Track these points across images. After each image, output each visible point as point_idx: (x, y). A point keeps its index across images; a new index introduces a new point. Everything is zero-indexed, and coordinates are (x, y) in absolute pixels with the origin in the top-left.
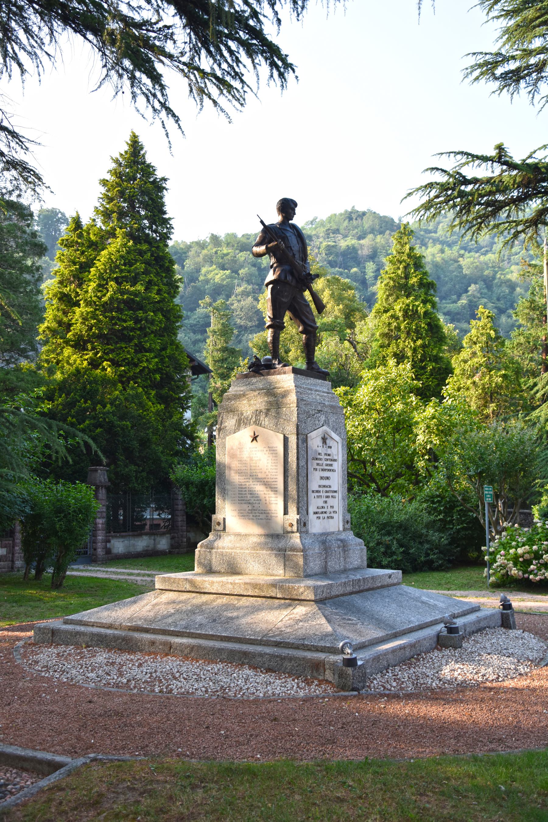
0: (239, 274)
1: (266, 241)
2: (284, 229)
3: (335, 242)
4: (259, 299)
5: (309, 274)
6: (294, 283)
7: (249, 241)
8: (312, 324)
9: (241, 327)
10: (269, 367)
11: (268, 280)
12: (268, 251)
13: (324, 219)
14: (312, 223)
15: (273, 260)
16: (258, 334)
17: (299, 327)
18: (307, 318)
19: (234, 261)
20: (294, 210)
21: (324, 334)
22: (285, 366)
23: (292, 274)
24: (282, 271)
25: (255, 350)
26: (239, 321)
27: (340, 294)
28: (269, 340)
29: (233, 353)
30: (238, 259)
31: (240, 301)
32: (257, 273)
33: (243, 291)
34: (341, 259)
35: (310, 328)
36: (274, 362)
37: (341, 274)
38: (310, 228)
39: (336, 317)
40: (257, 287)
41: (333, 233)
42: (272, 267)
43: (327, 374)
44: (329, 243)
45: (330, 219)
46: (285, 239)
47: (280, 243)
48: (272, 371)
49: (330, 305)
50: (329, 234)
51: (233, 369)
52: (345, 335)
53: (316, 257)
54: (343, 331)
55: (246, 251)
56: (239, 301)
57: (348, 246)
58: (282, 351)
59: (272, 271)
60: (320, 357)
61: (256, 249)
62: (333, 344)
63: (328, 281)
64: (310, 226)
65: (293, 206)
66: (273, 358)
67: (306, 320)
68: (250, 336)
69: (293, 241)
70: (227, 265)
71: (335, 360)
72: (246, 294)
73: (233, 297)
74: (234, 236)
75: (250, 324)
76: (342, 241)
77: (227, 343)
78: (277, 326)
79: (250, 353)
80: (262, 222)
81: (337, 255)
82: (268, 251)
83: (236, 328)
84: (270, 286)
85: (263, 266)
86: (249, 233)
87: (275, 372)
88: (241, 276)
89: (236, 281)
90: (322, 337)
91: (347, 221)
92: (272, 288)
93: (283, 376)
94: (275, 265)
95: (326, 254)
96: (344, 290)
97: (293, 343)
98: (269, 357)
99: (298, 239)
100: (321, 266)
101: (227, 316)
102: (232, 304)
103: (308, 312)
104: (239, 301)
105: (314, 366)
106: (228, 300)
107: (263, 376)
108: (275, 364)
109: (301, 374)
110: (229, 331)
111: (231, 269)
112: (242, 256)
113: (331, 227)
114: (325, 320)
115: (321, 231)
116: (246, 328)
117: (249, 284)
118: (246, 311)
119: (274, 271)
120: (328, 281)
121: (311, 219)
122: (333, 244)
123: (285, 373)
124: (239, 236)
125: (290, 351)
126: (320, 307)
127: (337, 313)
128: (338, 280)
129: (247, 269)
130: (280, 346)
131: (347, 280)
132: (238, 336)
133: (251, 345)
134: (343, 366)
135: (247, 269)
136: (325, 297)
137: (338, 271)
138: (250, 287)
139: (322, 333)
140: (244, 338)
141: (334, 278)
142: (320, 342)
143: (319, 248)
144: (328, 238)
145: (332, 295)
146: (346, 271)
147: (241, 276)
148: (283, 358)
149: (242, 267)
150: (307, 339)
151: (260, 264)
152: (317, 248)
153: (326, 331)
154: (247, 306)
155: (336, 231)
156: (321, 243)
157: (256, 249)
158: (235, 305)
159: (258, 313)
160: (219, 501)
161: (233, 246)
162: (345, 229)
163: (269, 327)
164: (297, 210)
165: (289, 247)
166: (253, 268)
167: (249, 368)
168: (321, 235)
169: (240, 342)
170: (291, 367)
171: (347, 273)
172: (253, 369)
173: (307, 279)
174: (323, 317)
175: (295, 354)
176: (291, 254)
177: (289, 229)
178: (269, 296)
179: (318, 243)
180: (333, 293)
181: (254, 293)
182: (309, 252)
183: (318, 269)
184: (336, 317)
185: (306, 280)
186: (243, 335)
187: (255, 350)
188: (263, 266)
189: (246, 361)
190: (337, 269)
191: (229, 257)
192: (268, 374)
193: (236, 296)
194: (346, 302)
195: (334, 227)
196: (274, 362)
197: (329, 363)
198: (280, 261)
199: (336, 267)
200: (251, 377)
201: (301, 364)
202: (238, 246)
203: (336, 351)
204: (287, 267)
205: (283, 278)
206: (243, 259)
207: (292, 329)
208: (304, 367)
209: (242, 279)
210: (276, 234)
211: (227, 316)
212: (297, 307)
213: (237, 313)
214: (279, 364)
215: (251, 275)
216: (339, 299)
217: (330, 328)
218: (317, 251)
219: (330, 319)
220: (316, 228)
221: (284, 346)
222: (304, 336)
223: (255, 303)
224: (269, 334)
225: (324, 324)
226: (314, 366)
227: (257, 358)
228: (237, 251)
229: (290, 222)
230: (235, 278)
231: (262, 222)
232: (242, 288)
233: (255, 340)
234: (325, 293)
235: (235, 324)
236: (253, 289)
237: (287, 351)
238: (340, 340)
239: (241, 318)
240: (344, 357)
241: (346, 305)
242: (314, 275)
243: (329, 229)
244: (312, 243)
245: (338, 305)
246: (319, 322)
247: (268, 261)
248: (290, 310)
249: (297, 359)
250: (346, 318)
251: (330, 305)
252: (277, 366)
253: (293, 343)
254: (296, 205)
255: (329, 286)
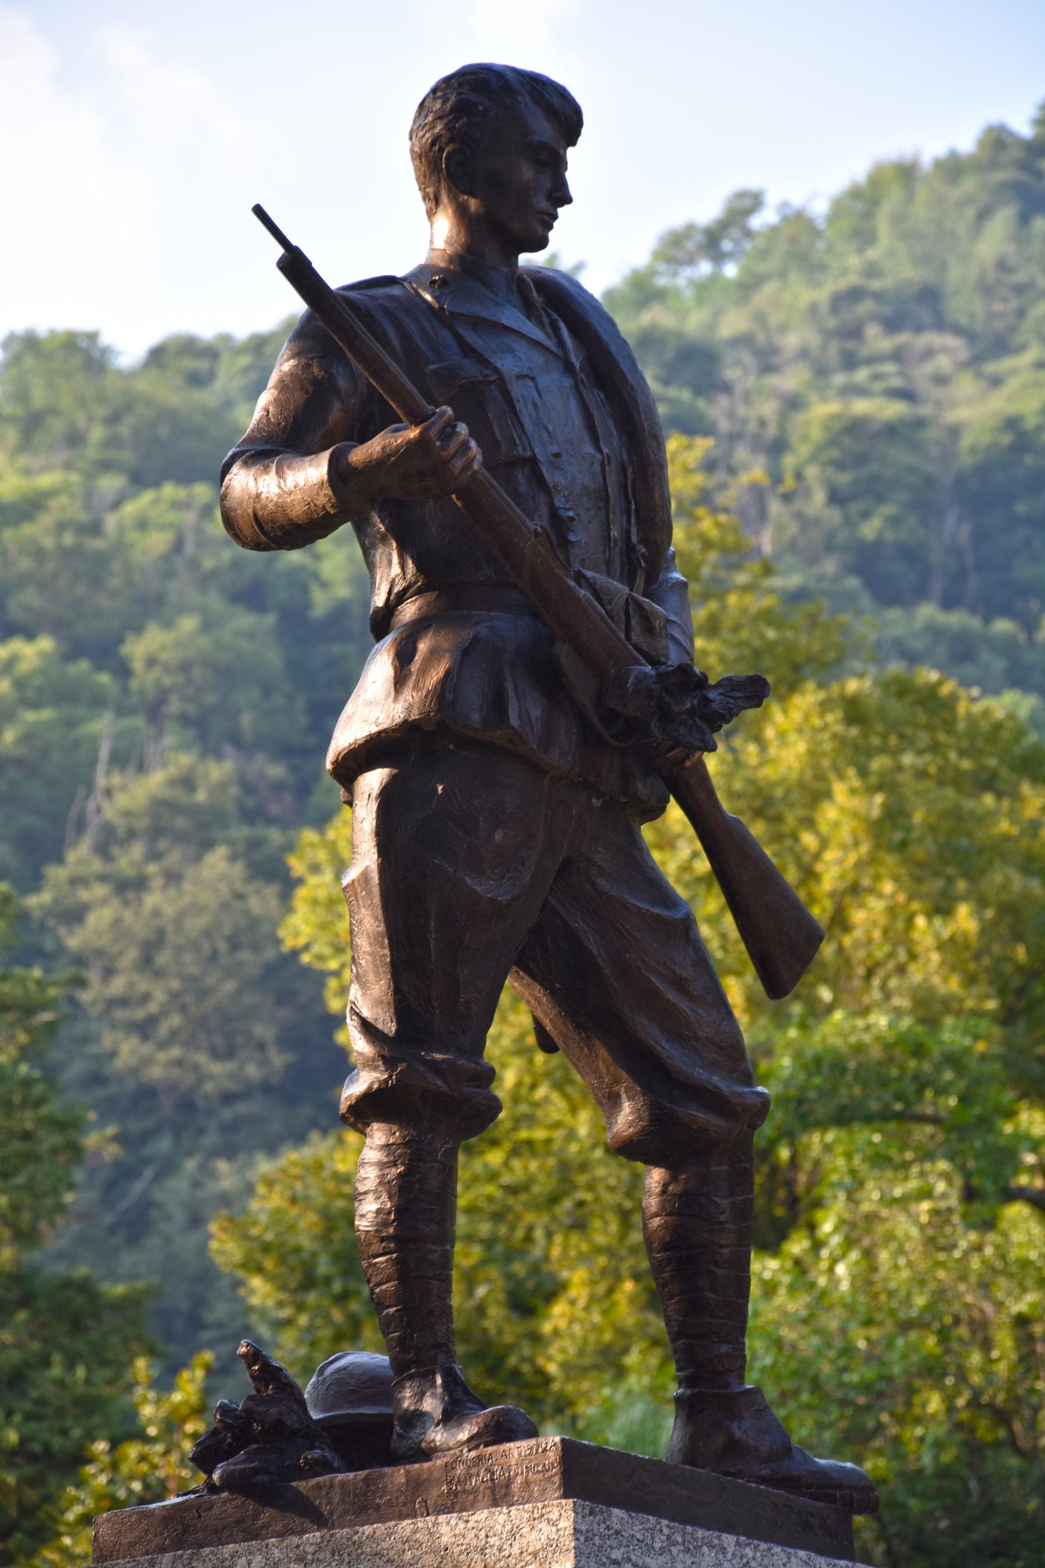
0: (123, 671)
1: (336, 413)
2: (479, 323)
3: (906, 395)
4: (297, 866)
5: (688, 679)
6: (562, 754)
7: (209, 397)
8: (717, 1081)
9: (146, 1095)
10: (371, 1440)
11: (351, 729)
12: (354, 498)
13: (819, 208)
14: (712, 241)
15: (392, 570)
16: (292, 1156)
17: (610, 1103)
18: (677, 1028)
19: (87, 559)
20: (559, 165)
21: (828, 1150)
22: (500, 1431)
23: (549, 681)
24: (465, 654)
25: (260, 1291)
26: (128, 1051)
27: (957, 815)
28: (369, 1211)
29: (77, 1326)
30: (121, 547)
31: (139, 884)
32: (274, 658)
33: (159, 806)
34: (955, 529)
35: (700, 1116)
36: (407, 1400)
37: (961, 652)
38: (703, 289)
39: (929, 1009)
40: (276, 771)
41: (892, 325)
42: (381, 623)
43: (855, 1496)
44: (861, 407)
45: (862, 205)
46: (482, 398)
47: (448, 432)
48: (398, 1475)
49: (877, 905)
50: (855, 332)
51: (80, 1458)
52: (1006, 1157)
53: (742, 521)
54: (986, 1123)
55: (185, 479)
56: (129, 887)
57: (1012, 423)
58: (475, 1294)
59: (380, 667)
60: (809, 1345)
61: (253, 485)
62: (906, 1227)
63: (854, 711)
64: (705, 268)
65: (544, 129)
66: (400, 1366)
67: (669, 1051)
68: (226, 1175)
69: (552, 410)
70: (30, 597)
71: (932, 1372)
72: (180, 827)
73: (80, 855)
74: (81, 353)
75: (218, 1073)
76: (966, 385)
77: (26, 1237)
78: (436, 1101)
79: (219, 1311)
80: (296, 267)
81: (924, 501)
82: (354, 498)
83: (108, 1109)
84: (373, 781)
85: (321, 602)
86: (206, 331)
87: (417, 1485)
88: (144, 679)
89: (102, 726)
90: (817, 1176)
91: (1003, 219)
92: (387, 797)
93: (486, 1519)
94: (409, 611)
95: (835, 497)
96: (987, 782)
97: (579, 1225)
98: (369, 1356)
99: (595, 398)
100: (796, 597)
101: (29, 1010)
102: (75, 915)
103: (680, 985)
104: (129, 887)
105: (742, 1430)
106: (33, 882)
107: (321, 1521)
108: (415, 1419)
109: (634, 1504)
110: (51, 1139)
111: (57, 627)
112: (152, 521)
113: (872, 271)
114: (837, 1029)
115: (793, 315)
116: (187, 1105)
117: (211, 750)
118: (191, 965)
119: (403, 658)
120: (854, 711)
121: (707, 212)
122: (894, 410)
123: (500, 1495)
124: (128, 346)
125: (553, 1291)
126: (785, 945)
127: (931, 970)
128: (934, 705)
129: (188, 624)
130: (465, 1256)
131: (1012, 705)
132: (125, 1172)
133: (224, 1247)
134: (1002, 1417)
135: (188, 624)
136: (832, 849)
137: (933, 630)
138: (218, 771)
139: (815, 1141)
140: (175, 1191)
141: (902, 689)
142: (798, 1210)
143: (778, 447)
144: (850, 362)
145: (889, 831)
146: (1003, 626)
147: (144, 679)
148: (491, 1357)
149: (150, 607)
150: (682, 1206)
151: (302, 582)
152: (757, 445)
153: (843, 1118)
154: (195, 924)
155: (919, 307)
156: (793, 403)
157: (253, 485)
158: (99, 919)
159: (293, 985)
160: (408, 615)
161: (75, 439)
162: (987, 290)
163: (367, 1110)
164: (580, 163)
165: (518, 466)
166: (245, 620)
167: (205, 1457)
168: (791, 341)
169: (136, 1225)
170: (552, 1438)
171: (1007, 647)
172: (237, 1463)
173: (665, 715)
174: (817, 1012)
175: (590, 1318)
176: (538, 523)
177: (512, 317)
178: (366, 858)
179: (768, 409)
180: (895, 815)
181: (251, 816)
182: (680, 482)
183: (767, 617)
184: (929, 1009)
185: (659, 723)
186: (168, 1167)
187: (260, 1291)
188: (321, 602)
189: (187, 1388)
190: (927, 612)
191: (38, 530)
192: (366, 1507)
193: (103, 850)
194: (1008, 880)
195: (903, 272)
196: (407, 1400)
197: (879, 1392)
198: (439, 575)
199: (920, 593)
200: (219, 1536)
201: (638, 1409)
202: (112, 442)
203: (941, 1294)
204: (507, 627)
205: (473, 710)
206: (158, 542)
207: (551, 1107)
208: (667, 1434)
209: (154, 711)
210: (412, 359)
211: (29, 1010)
212: (592, 944)
213: (117, 986)
214: (451, 1416)
215: (228, 674)
216: (941, 861)
217: (875, 1096)
218: (756, 472)
219: (881, 1021)
220: (747, 286)
221: (502, 1252)
222: (655, 1177)
223: (262, 900)
224: (368, 1157)
225: (829, 1066)
226: (742, 1430)
227: (268, 1375)
228: (110, 483)
229: (525, 259)
230: (98, 701)
231: (296, 267)
232: (156, 781)
233: (265, 1204)
234: (829, 814)
235: (96, 1079)
236: (248, 787)
237: (529, 1299)
238: (970, 1195)
239: (145, 1028)
240: (1004, 1341)
241: (1007, 909)
242: (729, 685)
243: (855, 294)
244: (717, 410)
245: (942, 908)
246: (780, 1047)
247: (362, 571)
248: (538, 971)
249: (609, 1361)
250: (1006, 1018)
251: (877, 905)
252: (438, 1436)
253: (579, 1225)
254: (564, 117)
255: (856, 755)
